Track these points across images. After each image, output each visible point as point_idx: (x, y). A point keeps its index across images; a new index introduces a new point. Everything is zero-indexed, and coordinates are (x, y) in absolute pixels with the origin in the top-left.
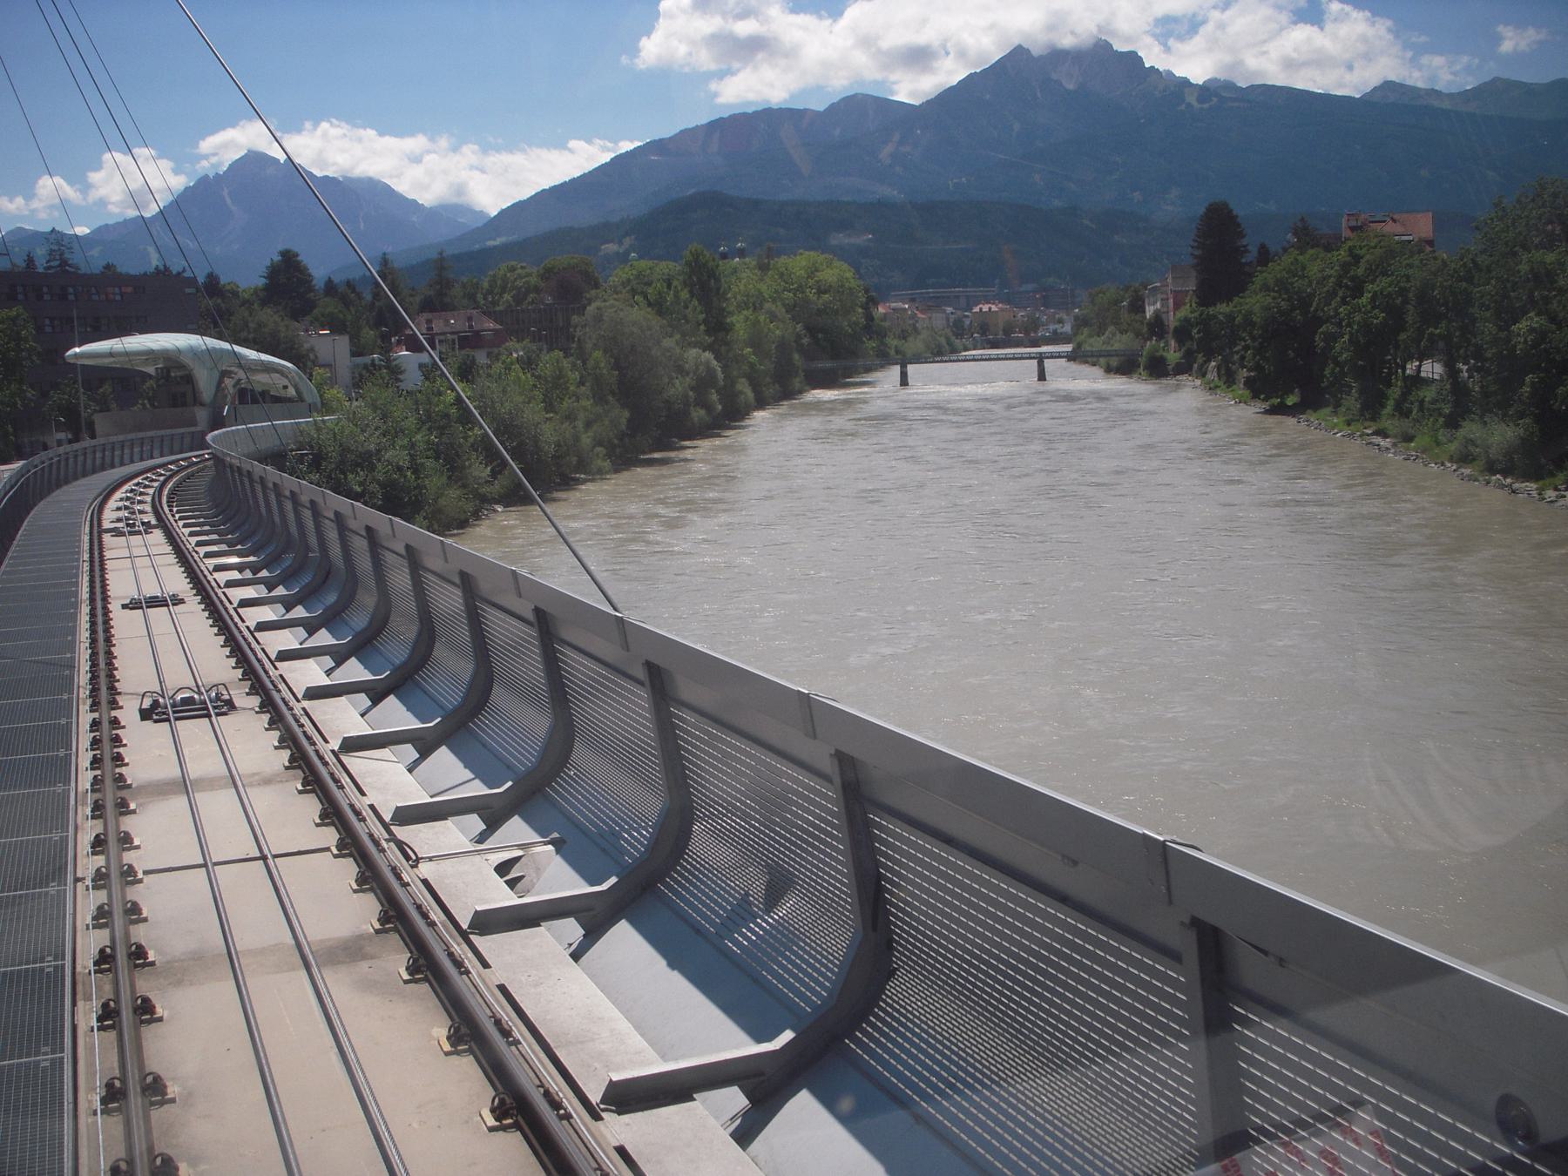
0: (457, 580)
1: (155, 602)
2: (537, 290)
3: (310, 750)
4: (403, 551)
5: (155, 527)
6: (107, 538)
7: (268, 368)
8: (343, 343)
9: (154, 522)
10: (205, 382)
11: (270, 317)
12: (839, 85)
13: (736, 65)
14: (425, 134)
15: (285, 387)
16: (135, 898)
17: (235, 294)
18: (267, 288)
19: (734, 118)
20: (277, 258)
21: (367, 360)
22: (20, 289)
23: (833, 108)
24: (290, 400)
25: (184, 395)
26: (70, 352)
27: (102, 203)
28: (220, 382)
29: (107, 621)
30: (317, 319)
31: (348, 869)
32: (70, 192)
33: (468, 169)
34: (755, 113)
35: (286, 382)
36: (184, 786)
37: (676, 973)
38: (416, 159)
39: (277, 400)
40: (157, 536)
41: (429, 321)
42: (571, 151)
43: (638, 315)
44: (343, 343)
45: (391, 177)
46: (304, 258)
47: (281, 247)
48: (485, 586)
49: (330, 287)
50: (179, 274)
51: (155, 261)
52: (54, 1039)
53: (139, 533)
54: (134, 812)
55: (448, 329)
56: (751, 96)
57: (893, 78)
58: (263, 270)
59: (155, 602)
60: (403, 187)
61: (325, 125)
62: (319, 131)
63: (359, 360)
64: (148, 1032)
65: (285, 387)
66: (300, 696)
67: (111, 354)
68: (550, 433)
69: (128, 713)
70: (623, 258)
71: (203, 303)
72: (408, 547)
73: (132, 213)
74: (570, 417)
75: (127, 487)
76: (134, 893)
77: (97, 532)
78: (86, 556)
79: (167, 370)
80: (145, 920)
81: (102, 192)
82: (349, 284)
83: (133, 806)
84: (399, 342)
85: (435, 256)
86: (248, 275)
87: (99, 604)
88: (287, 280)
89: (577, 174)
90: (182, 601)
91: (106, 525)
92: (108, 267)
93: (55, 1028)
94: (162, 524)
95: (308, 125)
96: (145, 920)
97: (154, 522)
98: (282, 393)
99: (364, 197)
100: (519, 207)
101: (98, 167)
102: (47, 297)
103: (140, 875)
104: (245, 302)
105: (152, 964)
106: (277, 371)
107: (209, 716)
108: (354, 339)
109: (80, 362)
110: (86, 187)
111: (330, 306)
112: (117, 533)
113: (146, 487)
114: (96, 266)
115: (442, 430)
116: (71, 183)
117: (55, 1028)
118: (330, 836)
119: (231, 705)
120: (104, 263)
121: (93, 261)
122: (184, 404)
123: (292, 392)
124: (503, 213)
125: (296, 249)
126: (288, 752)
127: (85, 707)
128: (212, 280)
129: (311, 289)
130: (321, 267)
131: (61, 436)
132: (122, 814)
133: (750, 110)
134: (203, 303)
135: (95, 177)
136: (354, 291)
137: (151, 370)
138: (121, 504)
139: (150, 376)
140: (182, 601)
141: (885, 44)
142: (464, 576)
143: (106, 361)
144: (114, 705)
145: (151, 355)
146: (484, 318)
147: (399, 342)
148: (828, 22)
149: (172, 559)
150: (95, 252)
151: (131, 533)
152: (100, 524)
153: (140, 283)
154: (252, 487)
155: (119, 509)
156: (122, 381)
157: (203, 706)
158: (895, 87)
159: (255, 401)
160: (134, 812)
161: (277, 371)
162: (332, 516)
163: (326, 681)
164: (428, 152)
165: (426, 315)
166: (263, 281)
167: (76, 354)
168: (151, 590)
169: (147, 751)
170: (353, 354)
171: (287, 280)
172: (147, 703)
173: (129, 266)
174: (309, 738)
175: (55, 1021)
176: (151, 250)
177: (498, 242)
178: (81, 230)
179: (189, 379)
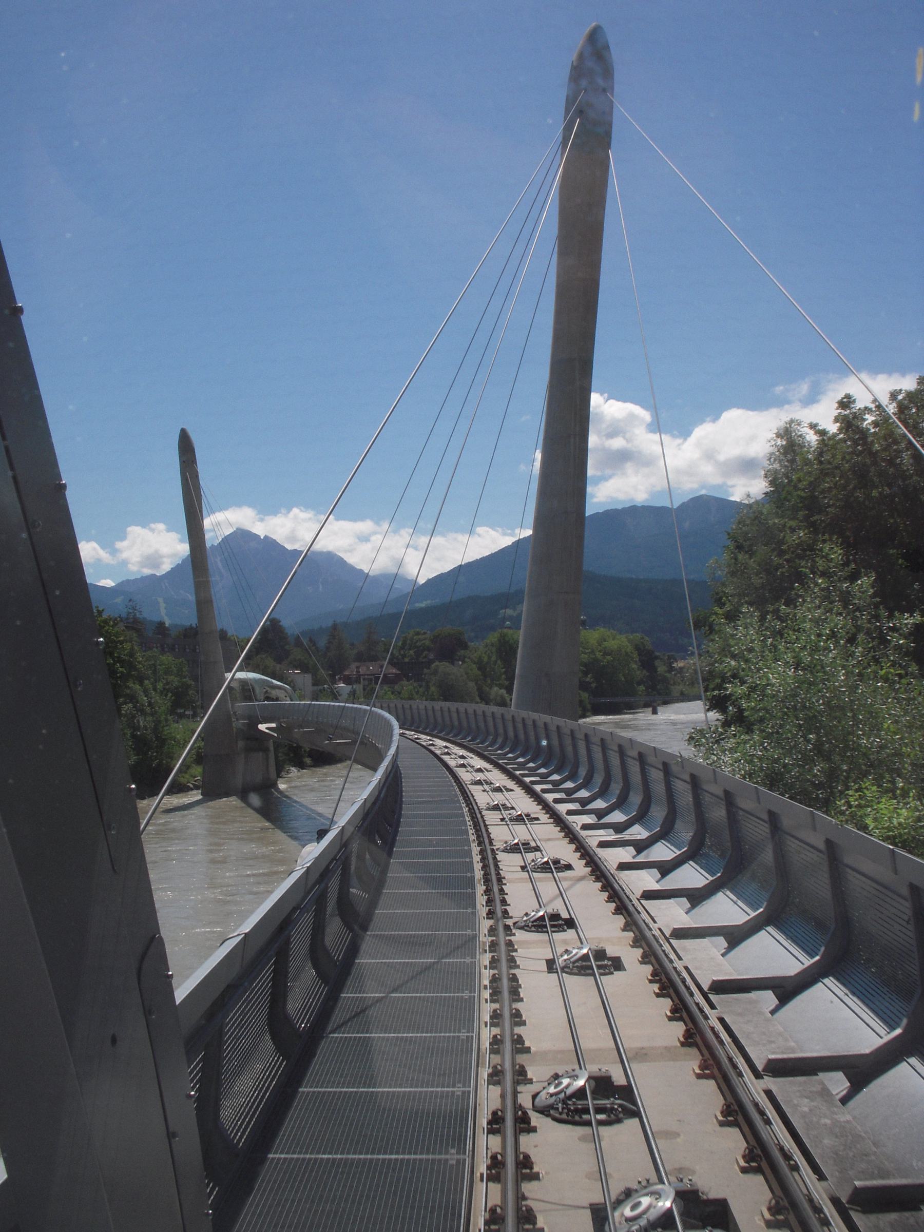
2: (429, 649)
7: (279, 688)
8: (308, 678)
12: (689, 487)
13: (608, 472)
14: (372, 519)
19: (607, 513)
21: (321, 687)
23: (684, 507)
27: (125, 563)
31: (692, 1062)
32: (103, 554)
34: (624, 509)
37: (713, 1195)
38: (364, 539)
41: (358, 668)
42: (479, 535)
44: (308, 678)
45: (346, 551)
55: (368, 673)
56: (621, 496)
57: (730, 483)
60: (352, 559)
61: (295, 510)
62: (291, 515)
63: (316, 688)
73: (147, 571)
81: (125, 555)
84: (340, 679)
85: (330, 623)
95: (283, 511)
99: (321, 567)
100: (441, 578)
101: (123, 538)
108: (314, 675)
110: (114, 552)
116: (103, 548)
118: (678, 1029)
126: (641, 951)
133: (620, 507)
135: (119, 545)
141: (722, 458)
147: (340, 679)
148: (679, 441)
150: (119, 600)
158: (731, 490)
162: (616, 748)
163: (657, 887)
164: (375, 533)
165: (357, 664)
170: (314, 685)
175: (456, 1182)
177: (423, 605)
178: (108, 583)
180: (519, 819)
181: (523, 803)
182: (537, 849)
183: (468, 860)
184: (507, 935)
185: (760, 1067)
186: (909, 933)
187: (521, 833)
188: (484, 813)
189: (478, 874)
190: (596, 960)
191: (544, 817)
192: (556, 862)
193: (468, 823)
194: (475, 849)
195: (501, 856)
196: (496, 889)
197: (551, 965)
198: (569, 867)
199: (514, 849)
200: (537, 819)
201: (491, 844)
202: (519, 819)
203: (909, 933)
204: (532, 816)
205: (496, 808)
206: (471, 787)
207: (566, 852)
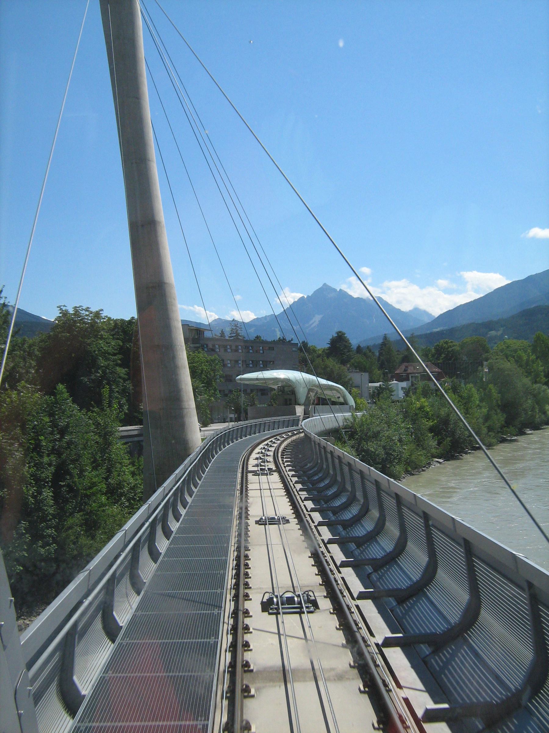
1: (272, 521)
3: (332, 577)
5: (274, 471)
6: (250, 475)
9: (274, 468)
10: (302, 394)
11: (332, 363)
15: (339, 398)
16: (248, 640)
17: (314, 351)
18: (329, 348)
24: (342, 404)
25: (290, 400)
26: (239, 377)
28: (308, 393)
29: (247, 530)
30: (353, 364)
33: (427, 292)
35: (339, 395)
36: (284, 675)
39: (334, 403)
40: (275, 477)
43: (508, 365)
46: (348, 336)
50: (289, 341)
51: (278, 335)
52: (216, 635)
53: (267, 475)
54: (253, 696)
55: (415, 371)
58: (328, 341)
59: (272, 521)
64: (248, 703)
65: (339, 398)
66: (355, 596)
67: (257, 379)
69: (253, 605)
70: (501, 338)
71: (301, 356)
75: (261, 446)
76: (247, 637)
77: (245, 472)
78: (239, 487)
79: (283, 387)
80: (251, 650)
82: (368, 347)
83: (253, 692)
86: (321, 343)
87: (244, 485)
88: (339, 344)
89: (463, 304)
90: (288, 521)
91: (250, 468)
92: (257, 337)
93: (206, 708)
94: (278, 470)
96: (251, 650)
97: (274, 468)
98: (337, 400)
102: (229, 350)
103: (251, 630)
104: (319, 356)
105: (252, 671)
107: (301, 613)
109: (242, 382)
111: (358, 358)
112: (255, 473)
113: (271, 446)
114: (252, 337)
115: (414, 421)
117: (206, 708)
119: (315, 604)
120: (256, 336)
121: (252, 334)
122: (290, 404)
123: (341, 400)
124: (441, 316)
125: (344, 331)
127: (238, 501)
128: (305, 344)
131: (232, 416)
132: (245, 697)
136: (370, 351)
137: (276, 387)
138: (258, 456)
139: (274, 389)
140: (288, 521)
144: (247, 518)
145: (276, 380)
149: (283, 492)
151: (263, 474)
152: (247, 468)
153: (272, 346)
154: (320, 450)
155: (257, 459)
156: (263, 389)
157: (298, 604)
160: (253, 696)
166: (329, 346)
167: (241, 379)
168: (270, 513)
169: (263, 647)
171: (339, 344)
172: (258, 519)
173: (268, 337)
174: (327, 562)
176: (277, 330)
177: (438, 330)
179: (293, 392)
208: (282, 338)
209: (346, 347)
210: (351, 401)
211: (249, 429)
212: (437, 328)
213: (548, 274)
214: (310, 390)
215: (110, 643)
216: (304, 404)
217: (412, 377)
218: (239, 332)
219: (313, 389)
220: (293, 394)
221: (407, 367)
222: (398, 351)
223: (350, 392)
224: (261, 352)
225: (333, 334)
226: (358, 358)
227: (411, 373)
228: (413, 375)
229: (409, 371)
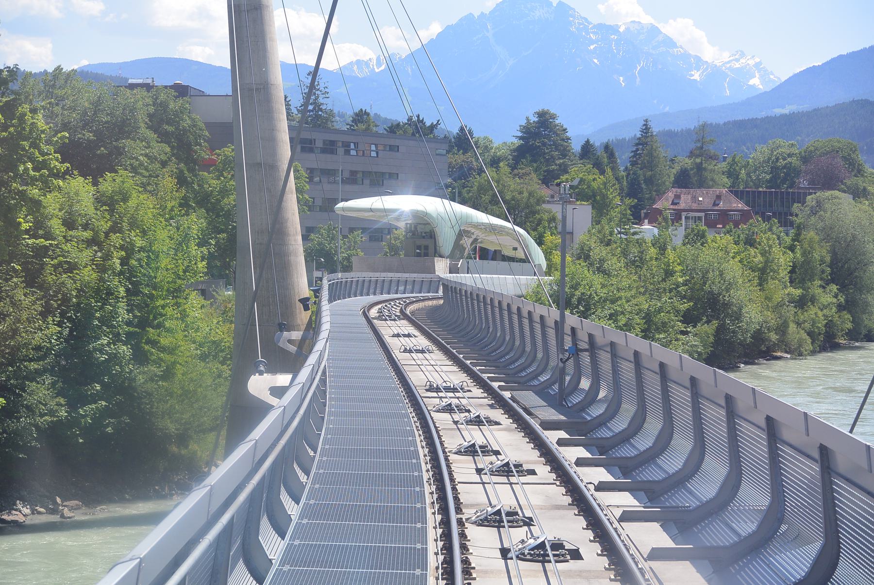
0: (816, 455)
4: (763, 424)
7: (492, 229)
10: (446, 239)
15: (515, 249)
20: (534, 119)
22: (352, 146)
25: (426, 248)
26: (341, 205)
35: (516, 245)
47: (539, 108)
48: (842, 463)
49: (587, 149)
55: (695, 206)
68: (754, 314)
71: (458, 165)
72: (769, 419)
74: (802, 303)
86: (502, 132)
88: (541, 142)
102: (353, 153)
104: (494, 162)
106: (508, 234)
122: (426, 255)
123: (520, 254)
129: (565, 152)
130: (580, 127)
134: (458, 165)
142: (824, 451)
143: (366, 215)
146: (732, 197)
156: (376, 231)
159: (494, 259)
161: (508, 234)
167: (343, 209)
171: (541, 142)
179: (431, 235)
180: (506, 470)
181: (513, 445)
182: (528, 522)
183: (419, 546)
184: (466, 579)
185: (645, 556)
186: (688, 401)
187: (504, 496)
188: (452, 457)
189: (434, 561)
190: (552, 550)
191: (544, 471)
192: (557, 546)
193: (424, 468)
194: (432, 519)
195: (472, 531)
196: (454, 517)
197: (505, 553)
198: (576, 555)
199: (495, 520)
200: (532, 472)
201: (459, 510)
202: (506, 470)
203: (688, 401)
204: (526, 467)
205: (471, 451)
206: (437, 416)
207: (572, 530)
208: (415, 119)
209: (557, 146)
210: (538, 255)
211: (386, 285)
212: (783, 107)
213: (873, 55)
214: (461, 234)
215: (279, 539)
216: (451, 256)
217: (687, 218)
218: (321, 100)
219: (468, 232)
220: (431, 237)
221: (678, 197)
222: (672, 160)
223: (540, 242)
224: (374, 154)
225: (528, 113)
226: (579, 172)
227: (685, 210)
228: (691, 214)
229: (682, 205)
